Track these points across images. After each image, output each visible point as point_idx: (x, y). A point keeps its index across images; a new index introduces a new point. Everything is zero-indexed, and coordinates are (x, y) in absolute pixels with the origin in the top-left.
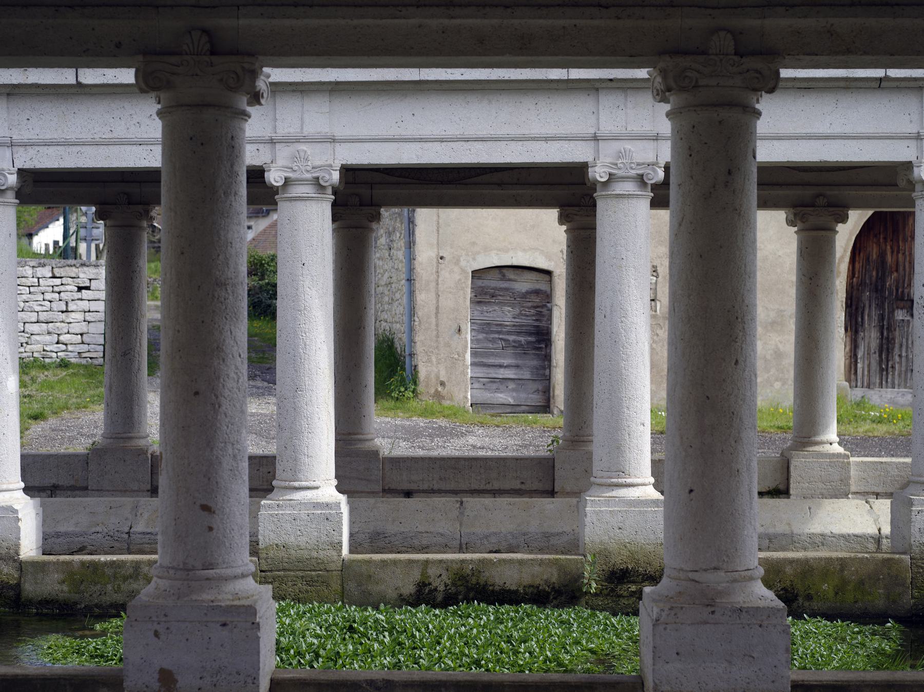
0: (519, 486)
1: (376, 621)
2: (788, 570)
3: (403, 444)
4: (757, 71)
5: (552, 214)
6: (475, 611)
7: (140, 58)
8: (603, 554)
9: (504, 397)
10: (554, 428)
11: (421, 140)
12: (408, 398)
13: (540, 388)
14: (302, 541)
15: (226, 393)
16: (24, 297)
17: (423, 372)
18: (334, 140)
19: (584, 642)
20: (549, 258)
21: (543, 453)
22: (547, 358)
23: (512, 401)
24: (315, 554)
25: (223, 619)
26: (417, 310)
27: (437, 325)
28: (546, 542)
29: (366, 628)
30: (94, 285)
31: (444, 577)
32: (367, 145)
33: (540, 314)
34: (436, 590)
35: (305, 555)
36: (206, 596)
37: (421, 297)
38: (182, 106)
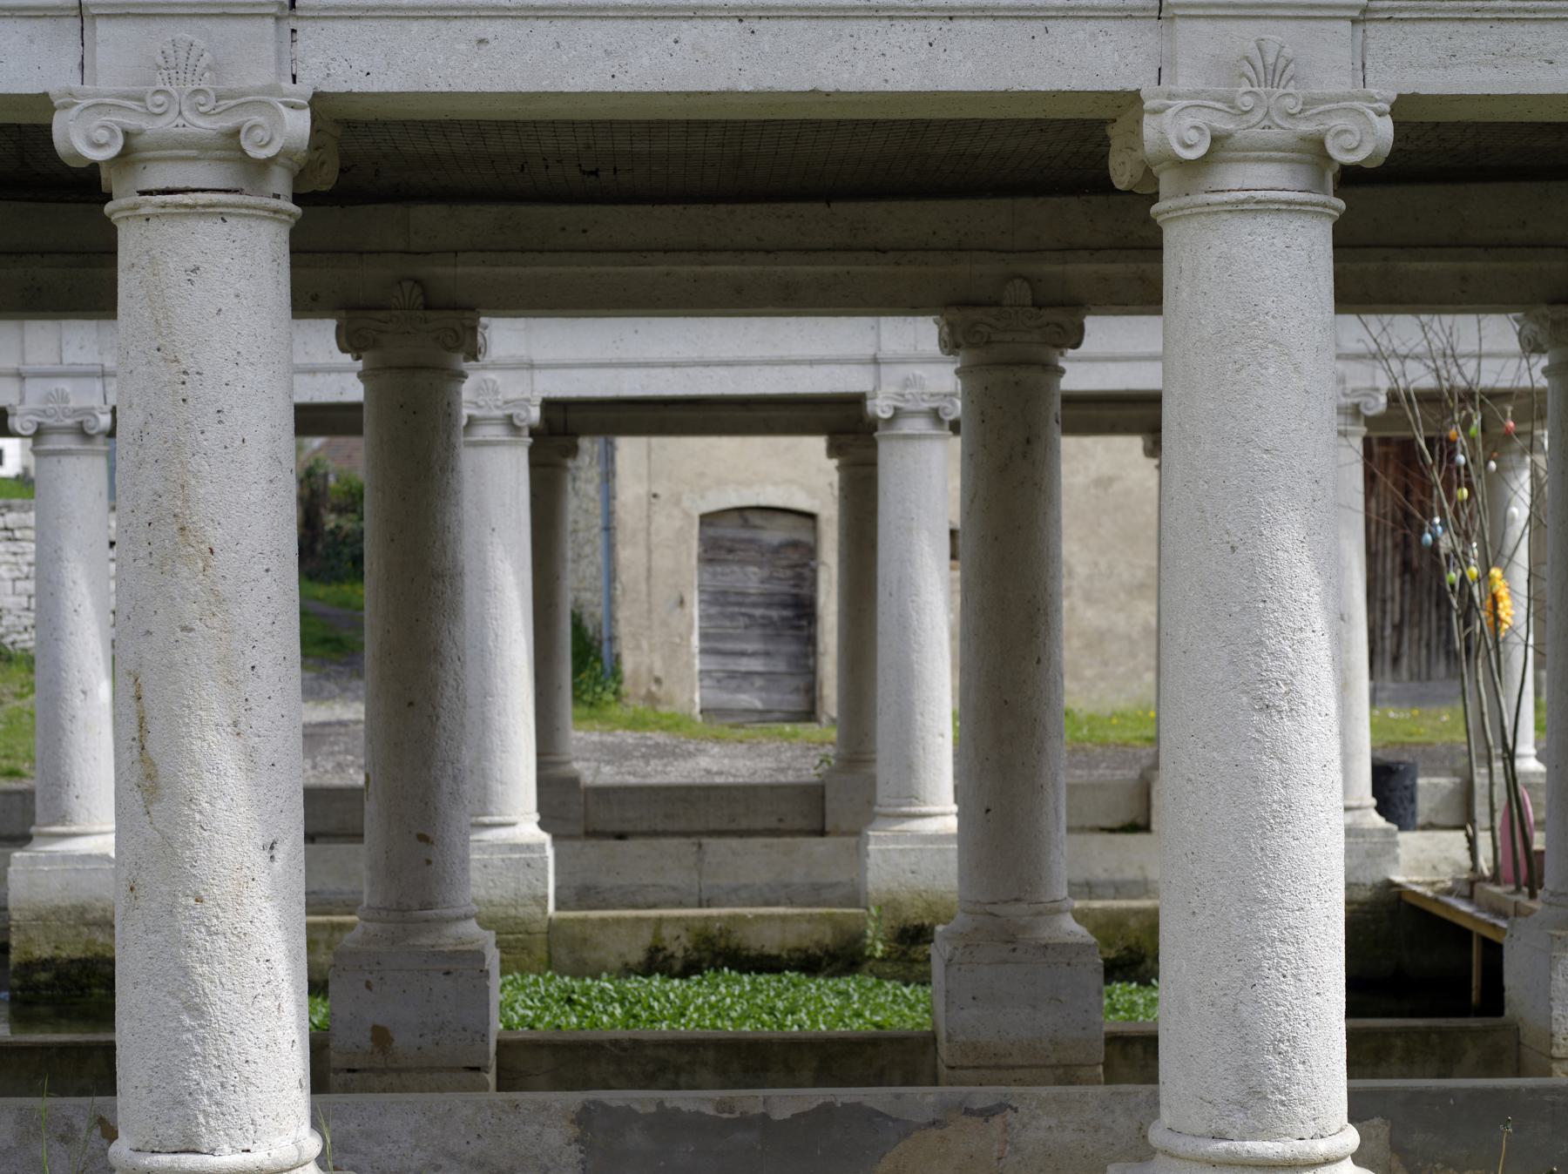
1: (602, 990)
2: (1133, 923)
3: (606, 769)
4: (1059, 325)
5: (819, 443)
6: (725, 981)
7: (343, 314)
8: (890, 905)
9: (750, 699)
10: (823, 744)
12: (608, 703)
14: (496, 894)
15: (445, 703)
17: (628, 665)
18: (531, 366)
19: (867, 1014)
22: (810, 641)
23: (759, 705)
24: (512, 912)
25: (446, 967)
27: (649, 594)
28: (816, 893)
29: (589, 1000)
31: (683, 940)
33: (799, 577)
34: (672, 956)
36: (425, 941)
37: (625, 554)
38: (391, 368)
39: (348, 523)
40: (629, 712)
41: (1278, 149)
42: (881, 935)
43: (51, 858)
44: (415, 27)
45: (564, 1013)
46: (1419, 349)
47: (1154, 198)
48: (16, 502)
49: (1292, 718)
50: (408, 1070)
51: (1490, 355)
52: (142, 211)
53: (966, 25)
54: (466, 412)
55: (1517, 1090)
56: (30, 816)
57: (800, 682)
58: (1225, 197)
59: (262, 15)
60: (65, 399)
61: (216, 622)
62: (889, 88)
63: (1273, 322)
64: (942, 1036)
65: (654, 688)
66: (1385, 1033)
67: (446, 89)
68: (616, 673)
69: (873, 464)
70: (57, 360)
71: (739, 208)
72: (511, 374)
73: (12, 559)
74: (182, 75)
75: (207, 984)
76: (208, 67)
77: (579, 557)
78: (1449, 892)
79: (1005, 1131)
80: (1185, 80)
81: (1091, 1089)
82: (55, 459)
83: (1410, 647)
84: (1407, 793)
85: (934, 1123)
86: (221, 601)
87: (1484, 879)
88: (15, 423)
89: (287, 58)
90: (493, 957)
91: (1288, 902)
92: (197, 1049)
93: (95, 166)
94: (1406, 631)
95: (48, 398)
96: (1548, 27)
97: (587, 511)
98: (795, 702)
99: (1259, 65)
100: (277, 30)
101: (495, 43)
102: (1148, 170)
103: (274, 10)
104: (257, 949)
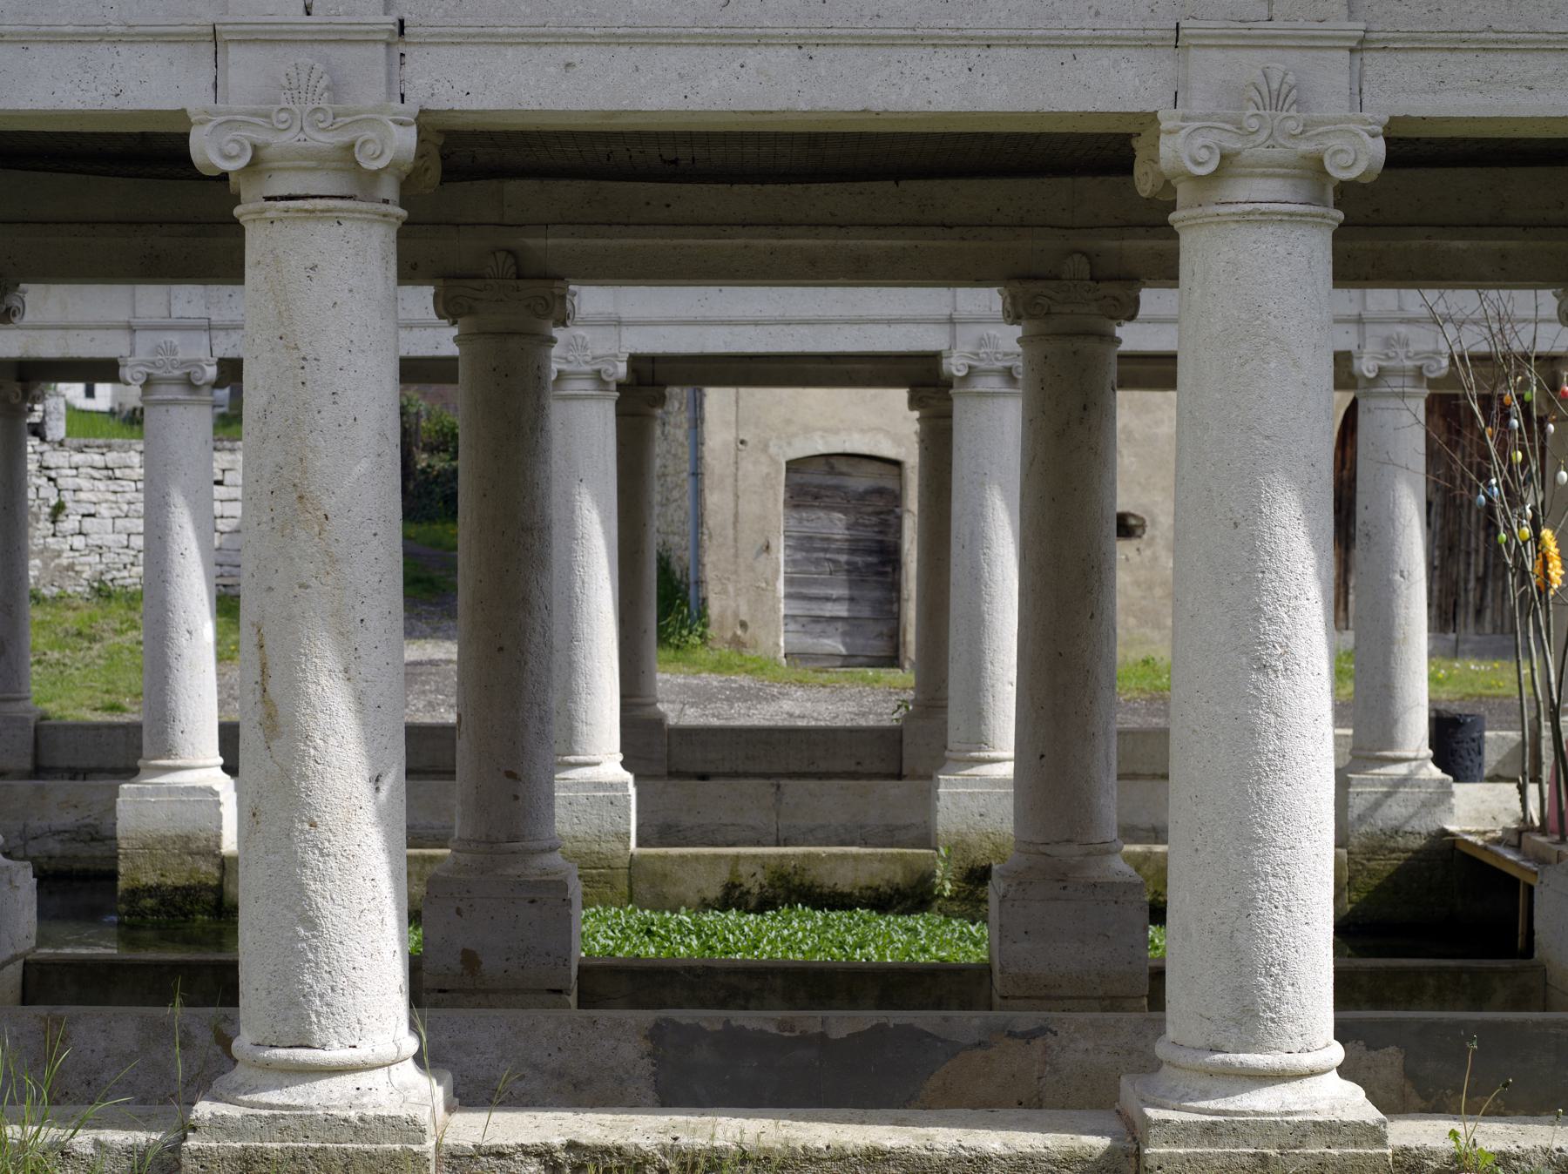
0: (853, 768)
1: (680, 923)
3: (690, 711)
4: (1115, 299)
7: (440, 282)
8: (959, 846)
9: (834, 644)
10: (904, 689)
11: (730, 323)
13: (885, 631)
16: (128, 496)
17: (714, 610)
18: (619, 323)
19: (933, 949)
20: (897, 441)
21: (887, 722)
22: (895, 587)
23: (843, 650)
24: (596, 847)
25: (531, 896)
26: (706, 518)
27: (736, 540)
29: (668, 931)
30: (228, 478)
32: (661, 329)
33: (884, 523)
34: (748, 892)
35: (584, 848)
37: (715, 500)
39: (440, 463)
40: (714, 656)
41: (1280, 166)
42: (949, 875)
43: (158, 790)
44: (510, 52)
45: (642, 944)
46: (1476, 316)
47: (1172, 206)
48: (116, 441)
49: (1286, 677)
50: (495, 991)
51: (1543, 321)
52: (267, 215)
53: (1002, 52)
54: (555, 367)
55: (1524, 1023)
56: (138, 751)
57: (883, 628)
58: (1233, 208)
59: (375, 41)
60: (174, 351)
61: (329, 580)
62: (932, 108)
63: (1275, 322)
64: (996, 967)
65: (739, 632)
66: (1418, 972)
67: (537, 108)
68: (702, 614)
69: (948, 416)
70: (166, 314)
71: (814, 187)
72: (600, 330)
73: (112, 497)
74: (303, 95)
75: (319, 899)
76: (327, 88)
77: (666, 503)
78: (1498, 841)
79: (1045, 1052)
80: (1197, 104)
81: (1135, 1015)
82: (163, 408)
83: (1493, 600)
84: (1474, 745)
85: (979, 1044)
86: (334, 561)
87: (1532, 829)
88: (125, 373)
89: (397, 78)
90: (576, 889)
91: (1280, 841)
92: (311, 956)
93: (224, 177)
94: (1490, 584)
95: (157, 350)
96: (1528, 57)
97: (675, 456)
98: (879, 647)
99: (1265, 90)
100: (388, 54)
101: (580, 67)
102: (1167, 182)
103: (385, 37)
104: (364, 870)
